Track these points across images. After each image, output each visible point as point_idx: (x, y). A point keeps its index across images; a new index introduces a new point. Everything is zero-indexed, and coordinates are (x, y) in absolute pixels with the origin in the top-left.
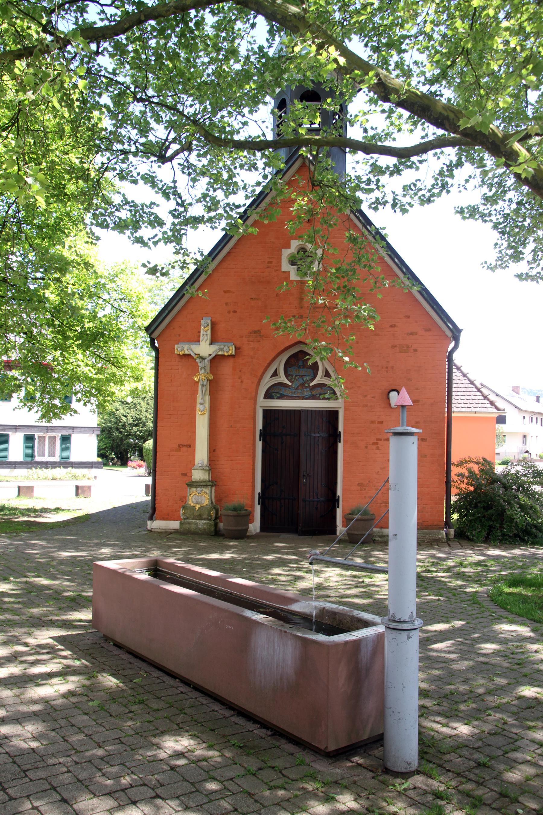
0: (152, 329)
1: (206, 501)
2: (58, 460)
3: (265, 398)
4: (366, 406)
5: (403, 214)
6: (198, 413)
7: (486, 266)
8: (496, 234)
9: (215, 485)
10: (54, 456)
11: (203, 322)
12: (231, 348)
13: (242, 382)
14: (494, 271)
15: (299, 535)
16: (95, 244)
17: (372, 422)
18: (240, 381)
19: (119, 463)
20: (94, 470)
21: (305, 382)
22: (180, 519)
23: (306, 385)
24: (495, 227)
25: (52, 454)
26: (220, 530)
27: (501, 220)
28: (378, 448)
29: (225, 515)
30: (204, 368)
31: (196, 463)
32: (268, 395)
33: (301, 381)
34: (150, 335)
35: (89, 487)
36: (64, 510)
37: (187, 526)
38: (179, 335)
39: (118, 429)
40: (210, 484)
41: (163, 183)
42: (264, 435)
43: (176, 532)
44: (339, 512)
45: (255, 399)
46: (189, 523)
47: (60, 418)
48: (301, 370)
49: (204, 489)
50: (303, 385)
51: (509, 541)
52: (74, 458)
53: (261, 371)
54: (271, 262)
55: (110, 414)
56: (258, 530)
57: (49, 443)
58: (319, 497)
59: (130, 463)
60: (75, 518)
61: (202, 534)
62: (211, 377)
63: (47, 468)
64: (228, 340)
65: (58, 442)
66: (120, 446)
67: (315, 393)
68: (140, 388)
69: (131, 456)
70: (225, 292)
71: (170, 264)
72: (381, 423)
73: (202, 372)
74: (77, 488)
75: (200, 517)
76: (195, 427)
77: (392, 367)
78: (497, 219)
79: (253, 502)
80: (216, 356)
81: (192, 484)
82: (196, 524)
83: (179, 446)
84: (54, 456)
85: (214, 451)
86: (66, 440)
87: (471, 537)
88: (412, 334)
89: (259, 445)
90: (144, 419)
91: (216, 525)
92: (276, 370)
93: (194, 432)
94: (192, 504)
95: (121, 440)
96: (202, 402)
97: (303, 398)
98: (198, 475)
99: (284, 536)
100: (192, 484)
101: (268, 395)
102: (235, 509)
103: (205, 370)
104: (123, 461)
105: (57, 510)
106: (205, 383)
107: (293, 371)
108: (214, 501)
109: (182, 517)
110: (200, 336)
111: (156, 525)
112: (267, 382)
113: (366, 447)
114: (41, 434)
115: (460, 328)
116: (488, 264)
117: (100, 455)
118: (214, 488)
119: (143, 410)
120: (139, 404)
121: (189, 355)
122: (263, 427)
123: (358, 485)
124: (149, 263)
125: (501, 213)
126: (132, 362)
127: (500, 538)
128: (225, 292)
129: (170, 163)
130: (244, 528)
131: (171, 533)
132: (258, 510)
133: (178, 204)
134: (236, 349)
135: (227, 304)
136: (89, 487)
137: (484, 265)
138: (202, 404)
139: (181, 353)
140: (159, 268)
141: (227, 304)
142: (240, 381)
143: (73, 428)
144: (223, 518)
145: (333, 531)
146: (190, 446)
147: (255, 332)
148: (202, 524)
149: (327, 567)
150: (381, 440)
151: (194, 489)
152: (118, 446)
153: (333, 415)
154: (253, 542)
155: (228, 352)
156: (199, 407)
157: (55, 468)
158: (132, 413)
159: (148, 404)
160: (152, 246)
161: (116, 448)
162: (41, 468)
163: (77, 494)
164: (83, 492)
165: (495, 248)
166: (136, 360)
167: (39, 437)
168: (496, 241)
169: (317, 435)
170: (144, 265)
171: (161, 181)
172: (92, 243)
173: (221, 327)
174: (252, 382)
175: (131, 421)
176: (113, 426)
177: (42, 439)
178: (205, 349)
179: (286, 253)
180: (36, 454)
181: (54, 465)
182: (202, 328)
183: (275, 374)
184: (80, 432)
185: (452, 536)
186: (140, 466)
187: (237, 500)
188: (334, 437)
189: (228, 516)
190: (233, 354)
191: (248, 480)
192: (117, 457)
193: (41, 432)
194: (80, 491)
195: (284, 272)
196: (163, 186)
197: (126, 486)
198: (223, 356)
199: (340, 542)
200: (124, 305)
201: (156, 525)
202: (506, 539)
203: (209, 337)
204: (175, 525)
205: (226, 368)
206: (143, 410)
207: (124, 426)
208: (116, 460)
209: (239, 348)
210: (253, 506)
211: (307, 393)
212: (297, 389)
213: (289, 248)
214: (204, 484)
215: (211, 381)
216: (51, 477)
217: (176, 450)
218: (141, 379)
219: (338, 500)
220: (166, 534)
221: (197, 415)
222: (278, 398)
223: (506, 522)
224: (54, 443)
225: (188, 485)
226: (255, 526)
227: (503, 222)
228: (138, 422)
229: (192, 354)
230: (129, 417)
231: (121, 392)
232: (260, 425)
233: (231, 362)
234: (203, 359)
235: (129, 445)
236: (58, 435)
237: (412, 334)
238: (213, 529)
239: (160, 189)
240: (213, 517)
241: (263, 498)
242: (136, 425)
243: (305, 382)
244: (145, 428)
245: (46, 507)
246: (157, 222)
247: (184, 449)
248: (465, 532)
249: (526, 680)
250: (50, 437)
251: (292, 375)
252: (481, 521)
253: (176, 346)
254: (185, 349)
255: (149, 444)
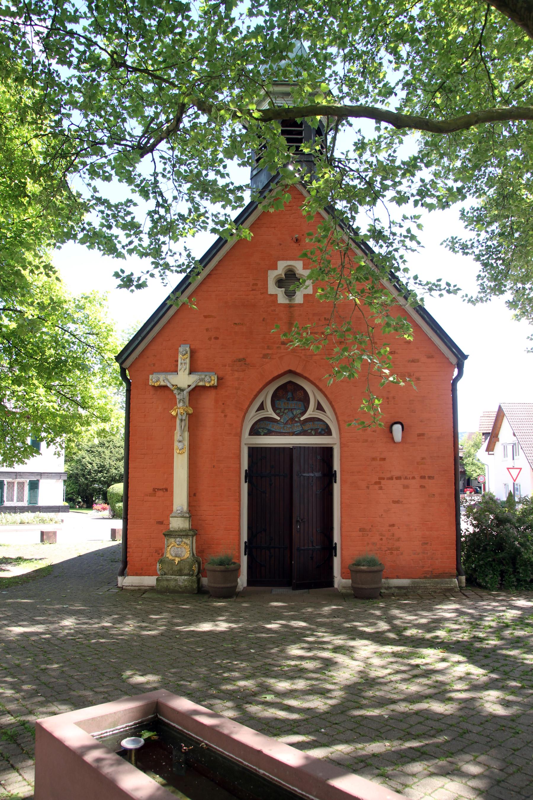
0: (124, 357)
1: (186, 554)
2: (27, 505)
3: (250, 434)
4: (366, 441)
5: (430, 211)
6: (176, 452)
7: (467, 299)
8: (478, 266)
9: (196, 534)
10: (23, 501)
11: (181, 349)
12: (213, 378)
13: (225, 416)
14: (475, 305)
15: (293, 589)
16: (59, 248)
17: (374, 459)
18: (223, 415)
19: (85, 506)
20: (61, 514)
21: (295, 416)
22: (156, 574)
23: (297, 419)
24: (478, 258)
25: (21, 499)
26: (202, 587)
27: (484, 253)
28: (381, 488)
29: (211, 571)
30: (183, 400)
31: (175, 508)
32: (254, 432)
33: (291, 415)
34: (121, 364)
35: (55, 533)
36: (26, 560)
37: (165, 583)
38: (154, 365)
39: (84, 475)
40: (191, 533)
41: (142, 178)
42: (249, 476)
43: (152, 589)
44: (337, 562)
45: (239, 435)
46: (167, 580)
47: (23, 462)
48: (290, 402)
49: (184, 540)
50: (292, 419)
51: (525, 587)
52: (42, 502)
53: (248, 403)
54: (256, 284)
55: (77, 462)
56: (245, 584)
57: (18, 488)
58: (314, 545)
59: (95, 506)
60: (36, 571)
61: (183, 592)
62: (191, 411)
63: (15, 513)
64: (209, 370)
65: (27, 488)
66: (85, 490)
67: (306, 428)
68: (107, 429)
69: (96, 499)
70: (205, 317)
71: (148, 272)
72: (384, 459)
73: (180, 405)
74: (42, 533)
75: (180, 573)
76: (172, 468)
77: (394, 398)
78: (480, 251)
79: (239, 552)
80: (197, 387)
81: (170, 534)
82: (176, 580)
83: (154, 490)
84: (23, 501)
85: (195, 495)
86: (34, 486)
87: (483, 584)
88: (413, 361)
89: (245, 487)
90: (108, 466)
91: (199, 580)
92: (262, 403)
93: (172, 474)
94: (170, 557)
95: (87, 484)
96: (181, 439)
97: (293, 434)
98: (177, 523)
99: (277, 590)
100: (170, 534)
101: (254, 432)
102: (221, 563)
103: (184, 402)
104: (89, 504)
105: (19, 560)
106: (184, 418)
107: (281, 404)
108: (195, 553)
109: (159, 573)
110: (177, 365)
111: (128, 581)
112: (253, 416)
113: (368, 487)
114: (10, 480)
115: (466, 354)
116: (469, 296)
117: (68, 499)
118: (195, 538)
119: (107, 457)
120: (103, 452)
121: (166, 387)
122: (249, 467)
123: (360, 530)
124: (123, 271)
125: (484, 244)
126: (99, 401)
127: (515, 583)
128: (205, 317)
129: (150, 154)
130: (233, 585)
131: (145, 591)
132: (244, 561)
133: (158, 205)
134: (219, 379)
135: (207, 330)
136: (55, 533)
137: (465, 298)
138: (180, 441)
139: (156, 385)
140: (135, 277)
141: (207, 330)
142: (223, 415)
143: (41, 474)
144: (208, 574)
145: (331, 584)
146: (166, 490)
147: (240, 360)
148: (183, 580)
149: (354, 639)
150: (383, 479)
151: (172, 540)
152: (84, 490)
153: (327, 453)
154: (245, 602)
155: (209, 382)
156: (177, 445)
157: (23, 512)
158: (97, 460)
159: (111, 452)
160: (127, 255)
161: (83, 492)
162: (9, 513)
163: (42, 540)
164: (49, 538)
165: (478, 280)
166: (104, 400)
167: (8, 483)
168: (478, 273)
169: (312, 475)
170: (117, 275)
171: (140, 175)
172: (55, 245)
173: (201, 355)
174: (237, 416)
175: (96, 468)
176: (80, 472)
177: (11, 484)
178: (183, 379)
179: (272, 275)
180: (5, 499)
181: (22, 510)
182: (180, 356)
183: (262, 407)
184: (48, 478)
185: (464, 585)
186: (104, 509)
187: (222, 552)
188: (329, 476)
189: (215, 571)
190: (216, 384)
191: (234, 528)
192: (83, 501)
193: (10, 478)
194: (45, 537)
195: (271, 295)
196: (142, 182)
197: (92, 532)
198: (204, 387)
199: (341, 596)
200: (91, 340)
201: (128, 581)
202: (522, 585)
203: (188, 366)
204: (150, 581)
205: (208, 402)
206: (107, 457)
207: (89, 473)
208: (82, 503)
209: (222, 379)
210: (239, 557)
211: (297, 428)
212: (286, 423)
213: (276, 269)
214: (184, 533)
215: (190, 415)
216: (19, 521)
217: (150, 495)
218: (109, 420)
219: (335, 548)
220: (140, 592)
221: (175, 455)
222: (265, 434)
223: (521, 566)
224: (23, 488)
225: (165, 535)
226: (243, 580)
227: (485, 254)
228: (102, 468)
229: (169, 385)
230: (95, 465)
231: (88, 436)
232: (245, 466)
233: (212, 394)
234: (181, 390)
235: (95, 490)
236: (26, 481)
237: (413, 361)
238: (195, 586)
239: (138, 186)
240: (196, 572)
241: (250, 548)
242: (101, 472)
243: (295, 416)
244: (108, 475)
245: (7, 557)
246: (133, 227)
247: (160, 493)
248: (476, 579)
249: (503, 723)
250: (18, 483)
251: (280, 409)
252: (491, 565)
253: (151, 376)
254: (161, 380)
255: (118, 488)
